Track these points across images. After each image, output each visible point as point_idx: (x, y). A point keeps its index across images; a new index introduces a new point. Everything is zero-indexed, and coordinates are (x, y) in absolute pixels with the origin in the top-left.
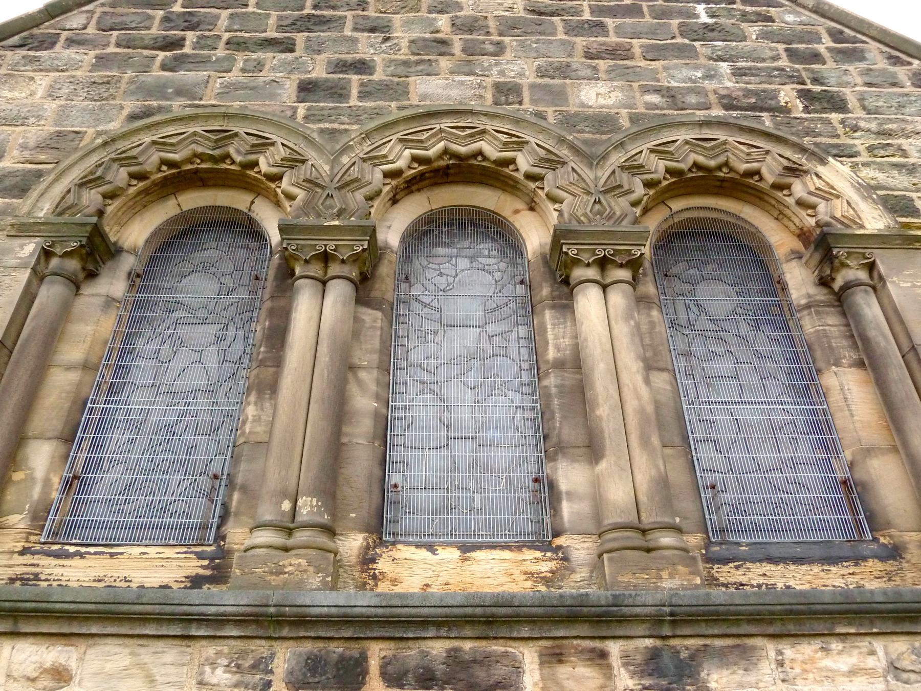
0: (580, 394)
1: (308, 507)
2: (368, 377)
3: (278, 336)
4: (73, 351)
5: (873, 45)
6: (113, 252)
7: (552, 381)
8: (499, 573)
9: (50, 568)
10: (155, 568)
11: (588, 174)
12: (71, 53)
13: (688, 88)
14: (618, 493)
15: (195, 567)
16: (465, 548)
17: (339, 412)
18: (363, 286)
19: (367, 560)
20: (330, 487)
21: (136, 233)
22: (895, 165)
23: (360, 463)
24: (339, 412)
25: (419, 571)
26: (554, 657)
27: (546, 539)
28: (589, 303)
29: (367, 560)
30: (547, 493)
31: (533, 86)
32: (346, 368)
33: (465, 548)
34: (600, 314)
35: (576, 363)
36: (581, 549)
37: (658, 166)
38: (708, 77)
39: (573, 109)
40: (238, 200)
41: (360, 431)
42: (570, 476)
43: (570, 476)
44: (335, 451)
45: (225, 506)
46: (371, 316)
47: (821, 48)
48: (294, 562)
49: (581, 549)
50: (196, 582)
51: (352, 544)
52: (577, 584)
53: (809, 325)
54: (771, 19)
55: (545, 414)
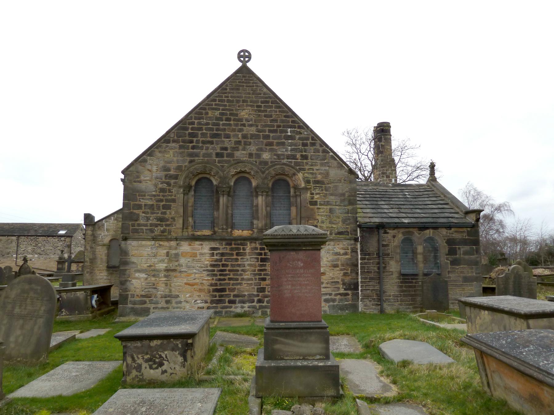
0: (257, 210)
1: (224, 227)
2: (230, 208)
3: (218, 201)
4: (190, 204)
5: (319, 141)
6: (191, 187)
7: (254, 208)
8: (246, 233)
9: (195, 233)
10: (207, 232)
11: (262, 175)
12: (174, 145)
13: (266, 230)
14: (260, 225)
15: (212, 233)
16: (242, 230)
17: (227, 214)
18: (229, 195)
19: (231, 232)
20: (227, 224)
21: (193, 183)
22: (311, 173)
23: (230, 220)
24: (227, 214)
25: (237, 233)
26: (251, 243)
27: (251, 229)
28: (260, 198)
29: (231, 232)
30: (252, 224)
31: (256, 154)
32: (227, 207)
33: (242, 230)
34: (260, 200)
35: (257, 206)
36: (255, 230)
37: (273, 173)
38: (286, 151)
39: (262, 160)
40: (208, 176)
41: (230, 215)
42: (255, 222)
43: (255, 222)
44: (227, 219)
45: (148, 170)
46: (230, 198)
47: (308, 142)
48: (224, 233)
49: (255, 230)
50: (212, 234)
51: (229, 230)
52: (255, 235)
53: (292, 199)
54: (301, 134)
55: (253, 213)
